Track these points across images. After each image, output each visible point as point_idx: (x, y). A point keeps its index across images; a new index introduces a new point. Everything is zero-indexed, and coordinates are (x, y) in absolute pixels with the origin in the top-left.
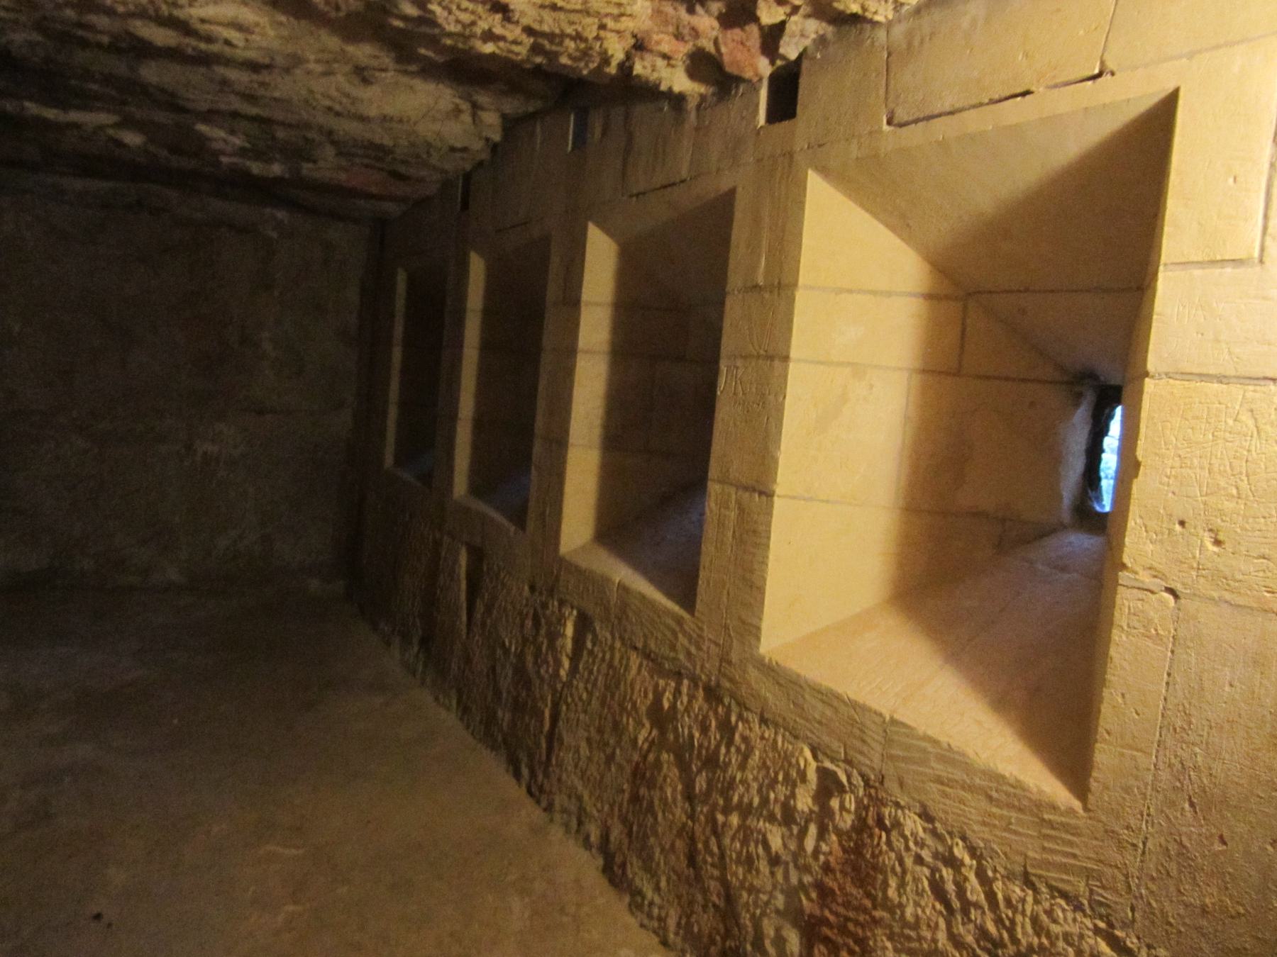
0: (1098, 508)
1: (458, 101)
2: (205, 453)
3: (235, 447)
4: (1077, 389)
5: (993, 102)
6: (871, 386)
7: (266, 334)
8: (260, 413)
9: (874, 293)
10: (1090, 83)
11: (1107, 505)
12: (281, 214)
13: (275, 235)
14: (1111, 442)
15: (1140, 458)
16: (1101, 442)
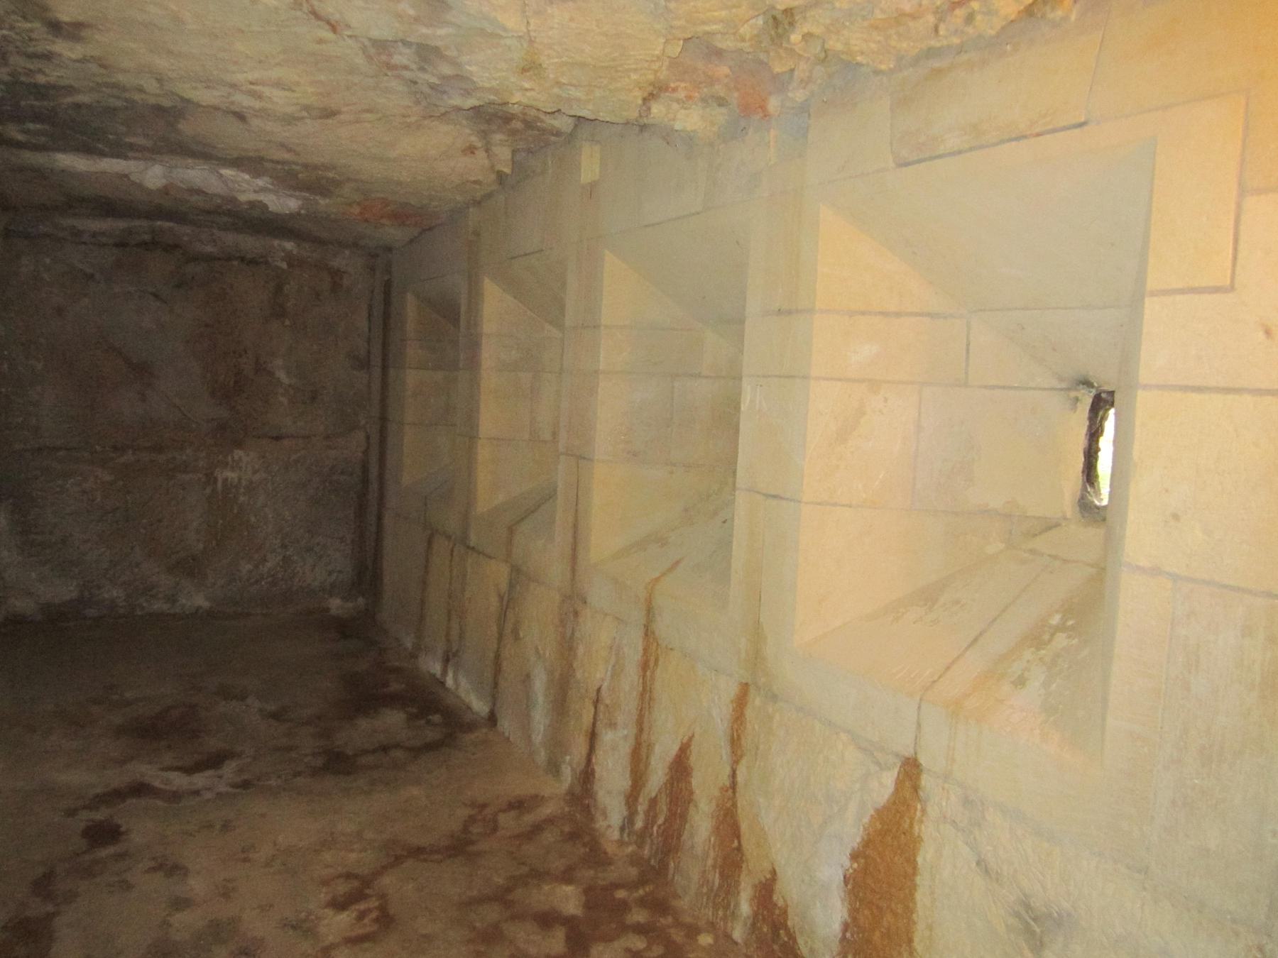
0: (1097, 503)
1: (473, 138)
2: (226, 479)
3: (255, 472)
4: (1073, 394)
5: (967, 358)
6: (886, 400)
7: (279, 362)
8: (278, 438)
9: (884, 314)
10: (1077, 131)
11: (1104, 499)
12: (289, 245)
13: (284, 265)
14: (1106, 444)
15: (128, 801)
16: (1097, 441)
